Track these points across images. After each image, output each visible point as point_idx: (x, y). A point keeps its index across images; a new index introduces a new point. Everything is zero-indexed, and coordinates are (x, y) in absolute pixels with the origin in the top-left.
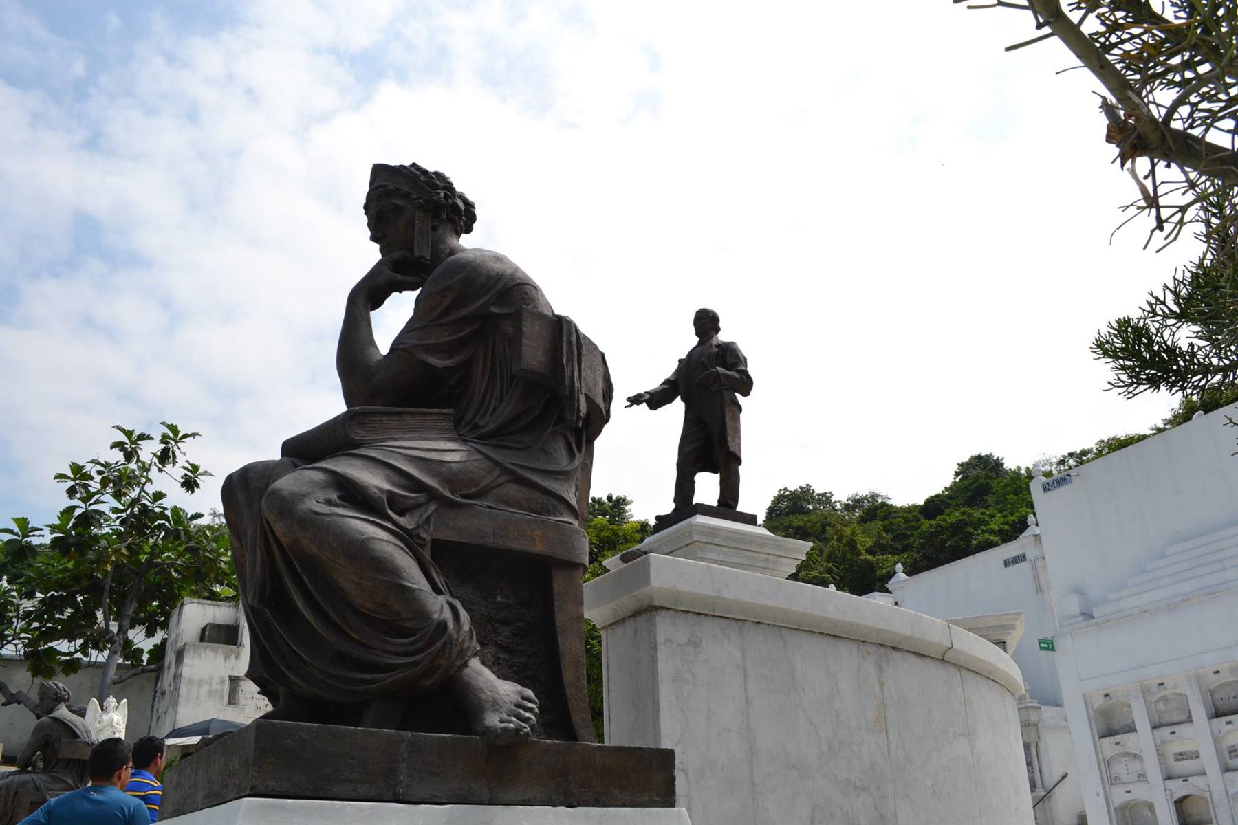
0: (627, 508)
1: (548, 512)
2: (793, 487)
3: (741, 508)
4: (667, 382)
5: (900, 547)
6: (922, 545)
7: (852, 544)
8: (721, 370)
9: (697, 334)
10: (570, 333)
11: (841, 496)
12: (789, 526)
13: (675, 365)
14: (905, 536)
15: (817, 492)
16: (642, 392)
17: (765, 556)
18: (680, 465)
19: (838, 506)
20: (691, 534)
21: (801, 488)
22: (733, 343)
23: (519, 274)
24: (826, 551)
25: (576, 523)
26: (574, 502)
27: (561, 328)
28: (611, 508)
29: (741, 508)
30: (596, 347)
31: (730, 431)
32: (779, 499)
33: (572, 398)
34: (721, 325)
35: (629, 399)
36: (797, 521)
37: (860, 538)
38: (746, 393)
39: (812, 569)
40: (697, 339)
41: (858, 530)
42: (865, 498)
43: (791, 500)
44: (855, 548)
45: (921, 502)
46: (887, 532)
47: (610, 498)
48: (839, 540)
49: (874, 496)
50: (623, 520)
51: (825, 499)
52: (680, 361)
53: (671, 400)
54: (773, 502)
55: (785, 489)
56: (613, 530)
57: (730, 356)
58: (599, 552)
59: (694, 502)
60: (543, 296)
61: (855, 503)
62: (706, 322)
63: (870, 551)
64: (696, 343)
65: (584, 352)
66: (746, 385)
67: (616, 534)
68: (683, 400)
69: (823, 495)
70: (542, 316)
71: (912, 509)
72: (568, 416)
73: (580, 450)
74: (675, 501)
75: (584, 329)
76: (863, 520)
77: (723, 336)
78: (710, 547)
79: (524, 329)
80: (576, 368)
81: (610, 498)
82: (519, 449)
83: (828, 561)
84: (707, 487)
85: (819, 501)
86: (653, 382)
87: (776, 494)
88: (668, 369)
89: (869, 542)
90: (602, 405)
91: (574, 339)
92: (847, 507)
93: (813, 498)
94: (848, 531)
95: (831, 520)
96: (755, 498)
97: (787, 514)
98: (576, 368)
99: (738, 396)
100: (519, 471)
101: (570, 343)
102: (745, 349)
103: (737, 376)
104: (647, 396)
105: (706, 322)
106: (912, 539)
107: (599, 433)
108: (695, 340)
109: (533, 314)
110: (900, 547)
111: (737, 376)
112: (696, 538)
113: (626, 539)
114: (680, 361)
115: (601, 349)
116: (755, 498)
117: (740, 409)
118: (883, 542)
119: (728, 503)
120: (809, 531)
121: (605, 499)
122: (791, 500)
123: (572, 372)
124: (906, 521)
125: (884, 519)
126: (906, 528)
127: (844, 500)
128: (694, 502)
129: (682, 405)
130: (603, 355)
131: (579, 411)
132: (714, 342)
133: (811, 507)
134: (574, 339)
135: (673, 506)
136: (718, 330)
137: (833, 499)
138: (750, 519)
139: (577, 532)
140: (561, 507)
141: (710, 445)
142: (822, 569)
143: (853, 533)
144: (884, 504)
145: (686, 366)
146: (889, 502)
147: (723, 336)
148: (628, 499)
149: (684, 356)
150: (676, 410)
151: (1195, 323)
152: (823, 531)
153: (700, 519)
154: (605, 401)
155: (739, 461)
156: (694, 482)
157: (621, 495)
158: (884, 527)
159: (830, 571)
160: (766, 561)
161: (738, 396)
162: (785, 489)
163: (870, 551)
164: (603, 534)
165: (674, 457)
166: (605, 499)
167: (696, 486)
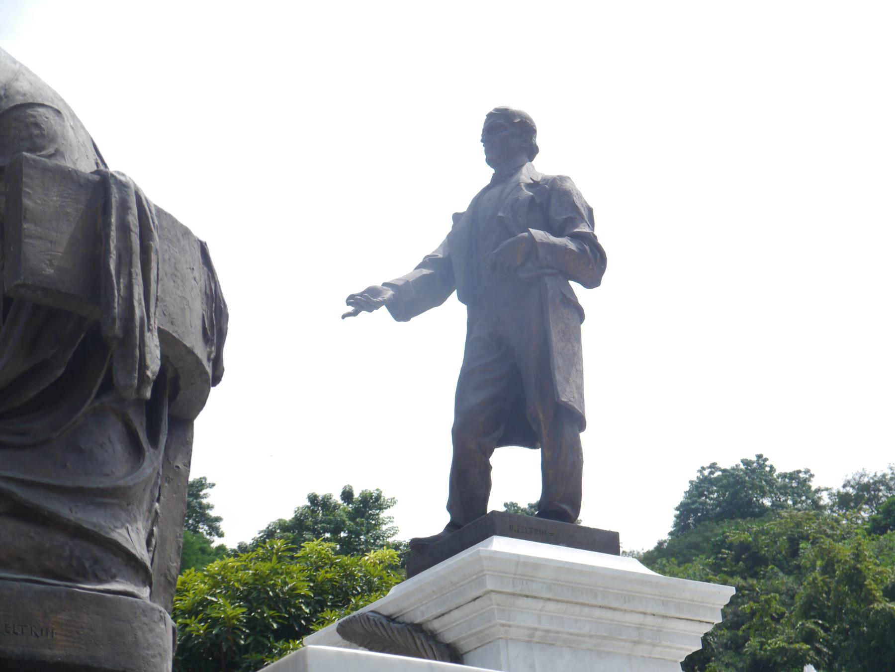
0: (384, 514)
1: (84, 575)
2: (729, 461)
3: (590, 516)
4: (429, 262)
8: (539, 234)
9: (490, 161)
10: (124, 207)
12: (722, 544)
13: (447, 227)
15: (780, 469)
17: (637, 619)
18: (460, 434)
19: (825, 500)
21: (746, 463)
23: (23, 85)
24: (802, 593)
25: (145, 592)
26: (141, 552)
27: (103, 193)
28: (353, 516)
30: (186, 232)
31: (558, 361)
32: (699, 488)
33: (130, 339)
34: (539, 140)
35: (352, 300)
36: (737, 533)
40: (491, 171)
42: (882, 481)
43: (725, 488)
44: (861, 586)
47: (347, 495)
48: (828, 569)
51: (798, 484)
52: (456, 217)
53: (439, 300)
55: (713, 466)
57: (557, 206)
58: (314, 613)
59: (489, 511)
60: (78, 125)
61: (861, 493)
62: (509, 137)
64: (487, 181)
65: (156, 242)
66: (591, 263)
67: (351, 576)
68: (462, 298)
69: (793, 476)
70: (69, 177)
72: (120, 378)
73: (154, 441)
74: (451, 507)
75: (157, 194)
76: (877, 528)
78: (522, 602)
79: (26, 201)
80: (138, 280)
81: (347, 495)
82: (21, 447)
83: (806, 614)
84: (516, 476)
85: (784, 490)
86: (402, 264)
87: (694, 476)
88: (432, 235)
90: (201, 351)
91: (133, 219)
92: (844, 501)
93: (771, 483)
94: (844, 550)
95: (809, 528)
96: (634, 490)
97: (719, 518)
98: (138, 280)
99: (575, 286)
100: (21, 493)
101: (124, 228)
102: (588, 190)
103: (572, 246)
104: (389, 293)
105: (509, 137)
108: (486, 174)
109: (45, 169)
111: (572, 246)
113: (369, 583)
114: (456, 217)
115: (199, 233)
116: (634, 490)
119: (556, 514)
121: (337, 498)
122: (725, 488)
123: (130, 287)
127: (837, 486)
128: (489, 511)
129: (463, 308)
130: (203, 249)
131: (143, 366)
133: (767, 502)
134: (133, 219)
135: (446, 518)
136: (532, 151)
137: (814, 485)
138: (607, 542)
139: (146, 611)
140: (114, 563)
141: (518, 393)
142: (792, 633)
147: (542, 166)
148: (386, 495)
150: (448, 326)
151: (207, 514)
152: (794, 552)
153: (501, 545)
155: (580, 423)
156: (488, 468)
157: (371, 488)
159: (809, 637)
160: (640, 628)
161: (575, 286)
162: (713, 466)
164: (321, 575)
165: (447, 418)
166: (337, 498)
167: (494, 475)
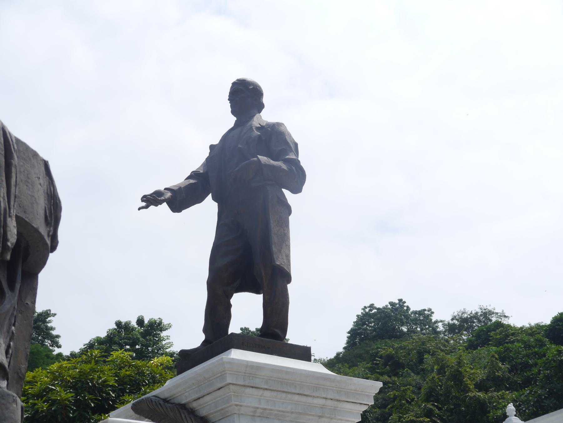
0: (164, 334)
2: (381, 303)
3: (293, 337)
4: (194, 175)
5: (519, 381)
6: (547, 377)
7: (457, 377)
8: (263, 159)
9: (233, 112)
11: (443, 315)
12: (376, 355)
13: (206, 153)
14: (526, 366)
15: (413, 308)
16: (162, 189)
17: (320, 402)
18: (212, 284)
19: (441, 328)
20: (223, 376)
21: (392, 304)
22: (279, 124)
24: (425, 386)
28: (144, 335)
29: (293, 337)
31: (275, 239)
32: (362, 320)
36: (386, 348)
37: (467, 369)
38: (297, 189)
39: (407, 411)
41: (466, 358)
42: (476, 316)
45: (547, 320)
46: (503, 360)
47: (140, 322)
48: (441, 371)
49: (487, 314)
50: (159, 351)
51: (424, 318)
52: (212, 147)
53: (199, 199)
54: (357, 323)
55: (372, 306)
56: (136, 367)
57: (276, 141)
58: (118, 397)
59: (229, 333)
61: (463, 323)
62: (245, 97)
63: (481, 386)
64: (232, 125)
65: (16, 160)
67: (142, 374)
68: (214, 199)
69: (421, 313)
71: (535, 331)
73: (12, 287)
74: (205, 330)
76: (472, 346)
77: (267, 116)
78: (249, 391)
81: (140, 322)
83: (427, 400)
84: (247, 311)
85: (416, 321)
86: (177, 177)
87: (360, 312)
88: (196, 158)
89: (481, 374)
90: (43, 230)
92: (451, 328)
93: (407, 317)
94: (452, 359)
95: (430, 346)
96: (321, 320)
97: (374, 339)
99: (286, 192)
102: (295, 130)
103: (284, 167)
104: (168, 195)
105: (245, 97)
106: (535, 370)
107: (44, 263)
108: (231, 121)
110: (519, 381)
111: (284, 167)
112: (229, 381)
113: (153, 378)
114: (212, 147)
116: (321, 320)
117: (288, 210)
118: (499, 374)
119: (272, 335)
120: (402, 360)
121: (134, 323)
124: (527, 346)
125: (499, 343)
126: (527, 356)
127: (448, 319)
128: (229, 333)
129: (215, 205)
132: (255, 122)
133: (405, 329)
136: (260, 107)
137: (434, 318)
138: (303, 353)
141: (249, 259)
143: (459, 363)
144: (499, 325)
145: (221, 154)
146: (505, 321)
147: (267, 116)
148: (165, 322)
149: (216, 141)
152: (421, 360)
154: (47, 222)
155: (288, 278)
156: (230, 306)
157: (156, 317)
158: (499, 353)
160: (323, 407)
161: (286, 192)
162: (372, 306)
163: (481, 386)
164: (123, 372)
166: (134, 323)
